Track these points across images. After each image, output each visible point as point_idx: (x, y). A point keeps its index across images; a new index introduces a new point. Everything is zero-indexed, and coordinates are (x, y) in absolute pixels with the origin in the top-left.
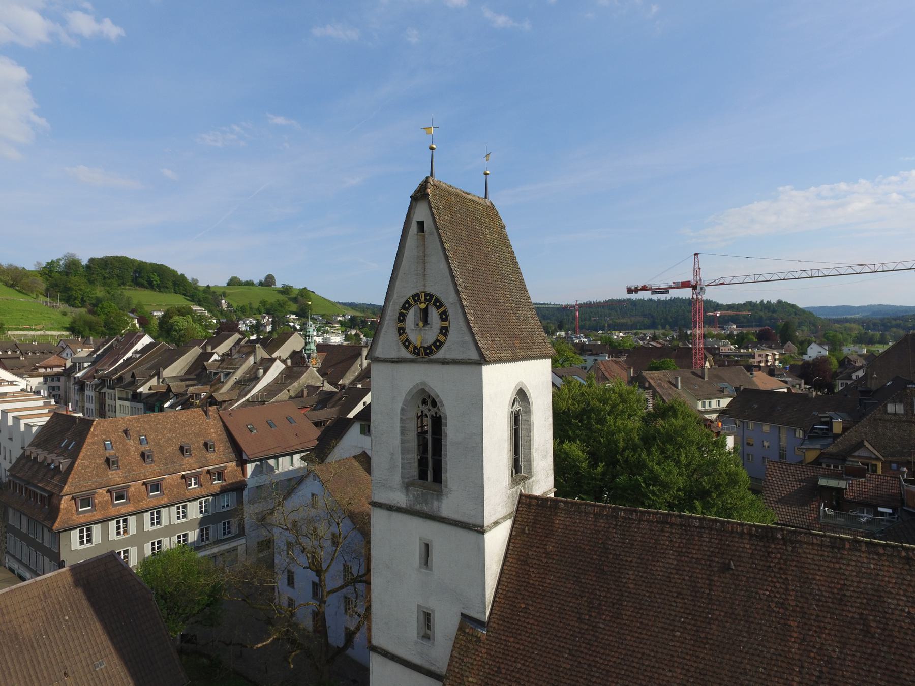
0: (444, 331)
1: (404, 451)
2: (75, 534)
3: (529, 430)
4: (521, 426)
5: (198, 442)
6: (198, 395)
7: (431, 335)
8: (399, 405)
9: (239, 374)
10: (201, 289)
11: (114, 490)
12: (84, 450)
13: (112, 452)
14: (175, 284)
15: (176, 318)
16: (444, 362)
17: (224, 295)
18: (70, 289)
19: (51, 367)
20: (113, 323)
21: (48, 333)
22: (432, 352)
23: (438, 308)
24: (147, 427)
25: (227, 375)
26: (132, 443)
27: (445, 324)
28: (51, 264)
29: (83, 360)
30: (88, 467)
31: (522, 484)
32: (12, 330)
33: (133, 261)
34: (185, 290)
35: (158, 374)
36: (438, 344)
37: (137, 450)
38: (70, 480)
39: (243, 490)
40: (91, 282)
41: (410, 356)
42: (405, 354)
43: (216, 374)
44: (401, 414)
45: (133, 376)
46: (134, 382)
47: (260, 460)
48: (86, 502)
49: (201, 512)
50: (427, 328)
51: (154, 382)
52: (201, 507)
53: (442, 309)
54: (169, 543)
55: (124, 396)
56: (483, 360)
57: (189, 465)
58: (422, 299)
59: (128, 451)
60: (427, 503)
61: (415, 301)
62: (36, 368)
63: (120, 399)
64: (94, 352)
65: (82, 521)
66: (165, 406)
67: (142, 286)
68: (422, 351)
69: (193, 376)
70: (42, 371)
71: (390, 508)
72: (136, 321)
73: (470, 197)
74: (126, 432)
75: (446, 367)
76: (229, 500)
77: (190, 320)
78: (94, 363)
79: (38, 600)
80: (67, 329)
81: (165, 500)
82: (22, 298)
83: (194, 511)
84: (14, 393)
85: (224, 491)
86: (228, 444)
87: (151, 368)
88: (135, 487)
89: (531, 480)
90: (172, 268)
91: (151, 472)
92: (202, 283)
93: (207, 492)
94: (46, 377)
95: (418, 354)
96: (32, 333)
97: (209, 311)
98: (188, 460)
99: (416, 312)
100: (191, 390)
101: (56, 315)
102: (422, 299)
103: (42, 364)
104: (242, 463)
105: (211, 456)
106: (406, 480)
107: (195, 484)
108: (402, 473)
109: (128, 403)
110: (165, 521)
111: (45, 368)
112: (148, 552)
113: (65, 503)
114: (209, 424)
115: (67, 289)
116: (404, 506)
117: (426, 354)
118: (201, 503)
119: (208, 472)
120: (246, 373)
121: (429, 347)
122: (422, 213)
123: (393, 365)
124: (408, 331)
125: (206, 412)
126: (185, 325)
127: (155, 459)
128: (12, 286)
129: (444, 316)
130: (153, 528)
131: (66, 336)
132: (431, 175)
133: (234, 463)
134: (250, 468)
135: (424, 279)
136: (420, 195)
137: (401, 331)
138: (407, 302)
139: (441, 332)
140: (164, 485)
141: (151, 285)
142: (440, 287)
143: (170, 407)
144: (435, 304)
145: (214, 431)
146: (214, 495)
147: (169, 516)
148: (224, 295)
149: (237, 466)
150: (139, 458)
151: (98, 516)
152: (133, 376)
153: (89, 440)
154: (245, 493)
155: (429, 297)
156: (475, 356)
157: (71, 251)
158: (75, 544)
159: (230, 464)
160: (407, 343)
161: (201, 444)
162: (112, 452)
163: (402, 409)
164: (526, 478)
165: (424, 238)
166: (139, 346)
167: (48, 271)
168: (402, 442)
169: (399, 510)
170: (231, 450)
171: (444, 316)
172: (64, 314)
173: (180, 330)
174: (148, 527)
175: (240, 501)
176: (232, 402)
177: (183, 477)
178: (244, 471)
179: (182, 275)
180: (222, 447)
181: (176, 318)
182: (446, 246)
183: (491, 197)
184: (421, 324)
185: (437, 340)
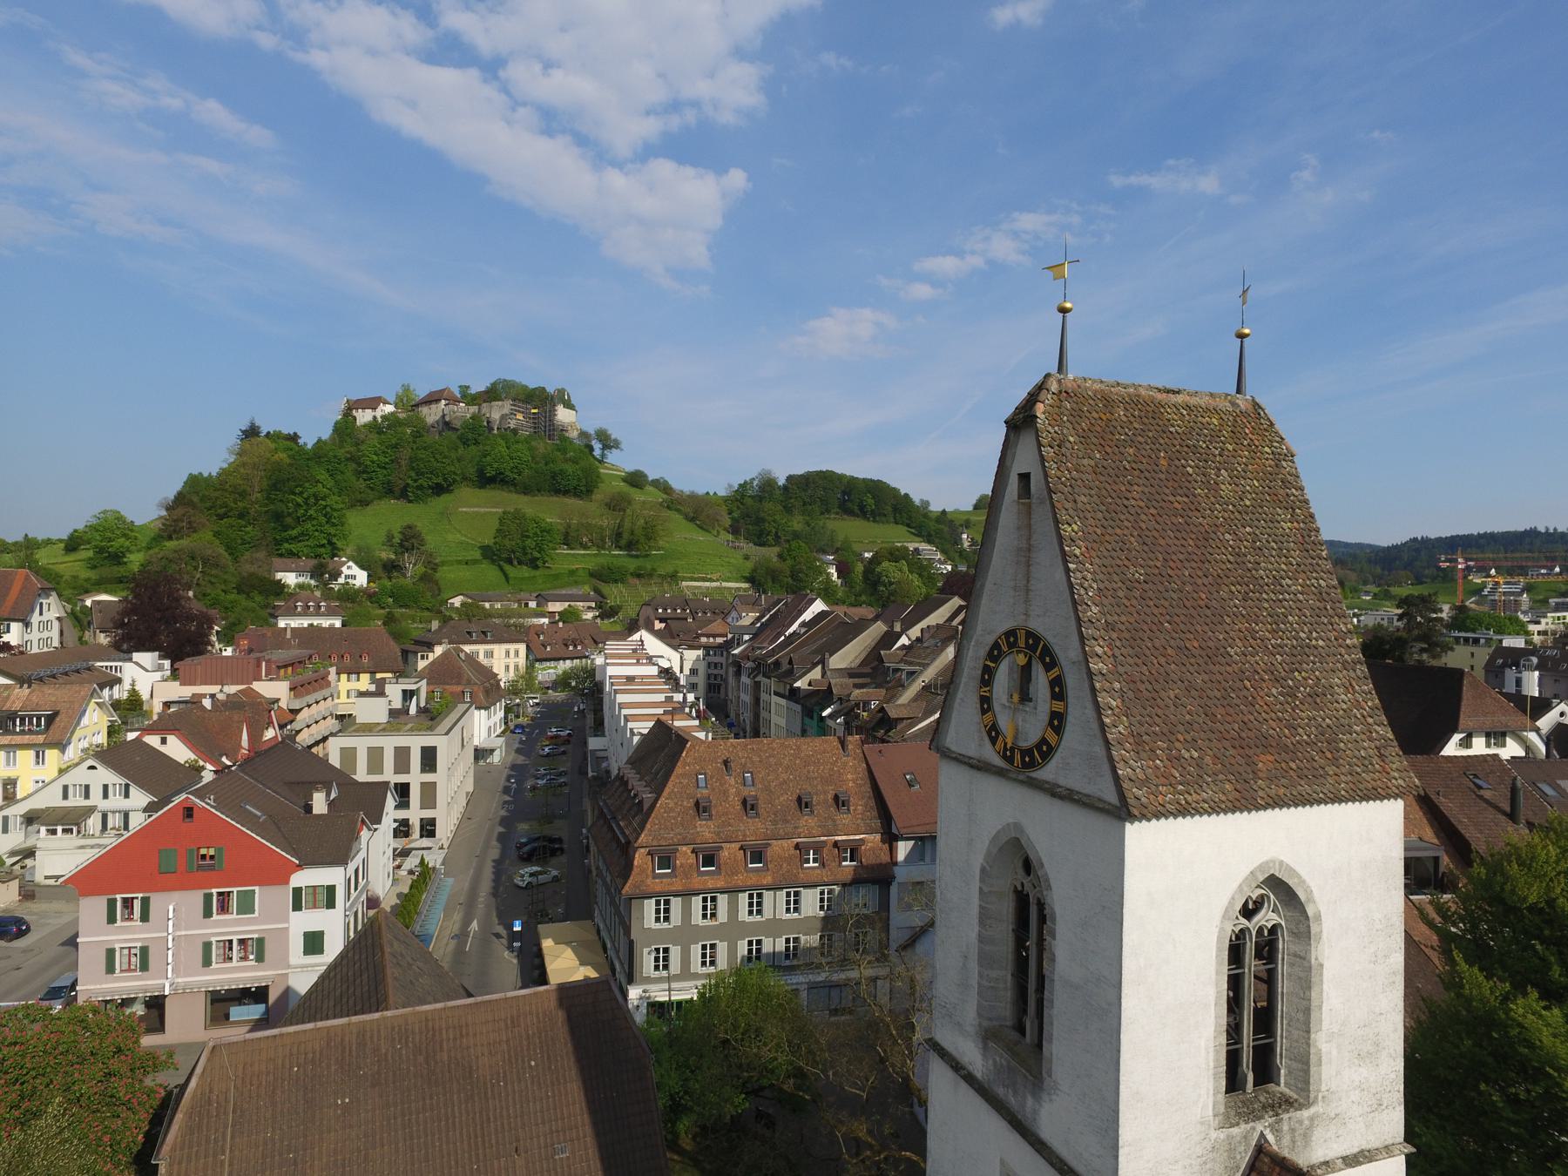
0: (1057, 722)
1: (985, 960)
2: (650, 905)
3: (1306, 979)
4: (1283, 968)
5: (825, 792)
6: (866, 703)
7: (1032, 727)
8: (978, 860)
9: (929, 675)
10: (933, 516)
11: (703, 850)
12: (670, 784)
13: (705, 791)
14: (895, 509)
15: (885, 564)
16: (1054, 791)
17: (967, 525)
18: (763, 520)
19: (714, 636)
20: (801, 571)
21: (725, 584)
22: (1032, 765)
23: (1048, 668)
24: (756, 759)
25: (911, 673)
26: (732, 781)
27: (1058, 706)
28: (743, 486)
29: (745, 630)
30: (672, 810)
31: (1269, 1120)
32: (684, 579)
33: (841, 477)
34: (910, 518)
35: (823, 662)
36: (1045, 750)
37: (738, 793)
38: (648, 826)
39: (889, 884)
40: (788, 510)
41: (991, 755)
42: (991, 755)
43: (896, 670)
44: (982, 880)
45: (790, 662)
46: (791, 674)
47: (921, 839)
48: (666, 862)
49: (822, 908)
50: (1028, 707)
51: (816, 674)
52: (822, 900)
53: (1054, 673)
54: (773, 945)
55: (781, 690)
56: (1123, 812)
57: (808, 827)
58: (1022, 643)
59: (725, 792)
60: (1015, 1092)
61: (1011, 646)
62: (698, 636)
63: (776, 694)
64: (758, 619)
65: (658, 889)
66: (825, 714)
67: (850, 513)
68: (1018, 757)
69: (867, 670)
70: (704, 640)
71: (956, 1066)
72: (833, 570)
73: (1179, 399)
74: (726, 763)
75: (1057, 803)
76: (864, 898)
77: (905, 568)
78: (755, 636)
79: (502, 1024)
80: (747, 580)
81: (768, 880)
82: (701, 537)
83: (811, 902)
84: (642, 677)
85: (857, 881)
86: (872, 803)
87: (815, 652)
88: (729, 852)
89: (1305, 1114)
90: (893, 484)
91: (752, 829)
92: (935, 507)
93: (831, 878)
94: (707, 648)
95: (1010, 760)
96: (707, 584)
97: (943, 552)
98: (808, 822)
99: (1011, 669)
100: (857, 694)
101: (736, 559)
102: (1022, 643)
103: (704, 630)
104: (891, 838)
105: (844, 819)
106: (986, 1023)
107: (815, 860)
108: (979, 1005)
109: (783, 702)
110: (768, 912)
111: (708, 636)
112: (742, 949)
113: (640, 858)
114: (845, 764)
115: (759, 521)
116: (979, 1075)
117: (1025, 766)
118: (822, 893)
119: (836, 844)
120: (941, 673)
121: (1028, 752)
122: (1025, 460)
123: (973, 772)
124: (996, 706)
125: (843, 743)
126: (898, 575)
127: (761, 811)
128: (692, 520)
129: (1058, 690)
130: (751, 919)
131: (745, 590)
132: (1061, 368)
133: (878, 836)
134: (903, 849)
135: (1027, 601)
136: (1021, 422)
137: (986, 704)
138: (996, 645)
139: (1051, 724)
140: (769, 853)
141: (863, 513)
142: (1051, 625)
143: (830, 716)
144: (1042, 659)
145: (851, 777)
146: (844, 885)
147: (775, 904)
148: (967, 525)
149: (883, 841)
150: (739, 807)
151: (678, 885)
152: (790, 662)
153: (678, 770)
154: (894, 889)
155: (1034, 639)
156: (1111, 797)
157: (768, 467)
158: (649, 921)
159: (871, 837)
160: (993, 733)
161: (830, 796)
162: (705, 791)
163: (983, 870)
164: (1288, 1103)
165: (1029, 506)
166: (807, 616)
167: (740, 496)
168: (981, 939)
169: (969, 1079)
170: (875, 813)
171: (1058, 690)
172: (747, 558)
173: (891, 583)
174: (743, 915)
175: (885, 905)
176: (915, 720)
177: (797, 846)
178: (892, 851)
179: (906, 495)
180: (861, 805)
181: (885, 564)
182: (1067, 530)
183: (1251, 388)
184: (1016, 697)
185: (1044, 741)
